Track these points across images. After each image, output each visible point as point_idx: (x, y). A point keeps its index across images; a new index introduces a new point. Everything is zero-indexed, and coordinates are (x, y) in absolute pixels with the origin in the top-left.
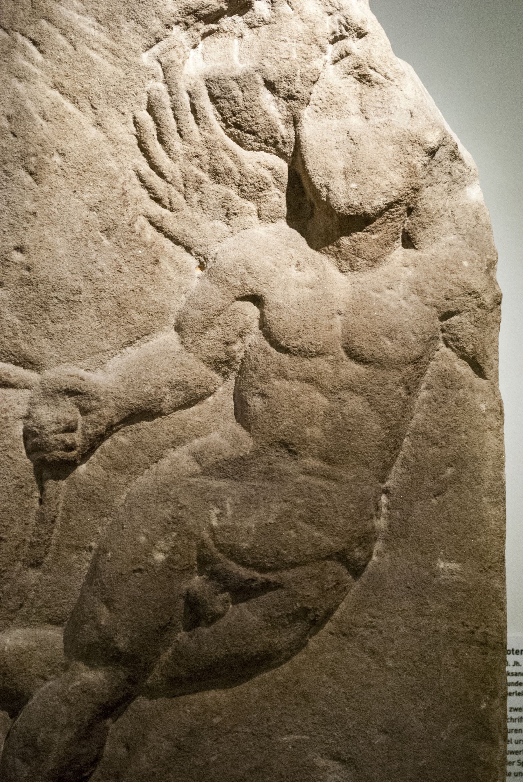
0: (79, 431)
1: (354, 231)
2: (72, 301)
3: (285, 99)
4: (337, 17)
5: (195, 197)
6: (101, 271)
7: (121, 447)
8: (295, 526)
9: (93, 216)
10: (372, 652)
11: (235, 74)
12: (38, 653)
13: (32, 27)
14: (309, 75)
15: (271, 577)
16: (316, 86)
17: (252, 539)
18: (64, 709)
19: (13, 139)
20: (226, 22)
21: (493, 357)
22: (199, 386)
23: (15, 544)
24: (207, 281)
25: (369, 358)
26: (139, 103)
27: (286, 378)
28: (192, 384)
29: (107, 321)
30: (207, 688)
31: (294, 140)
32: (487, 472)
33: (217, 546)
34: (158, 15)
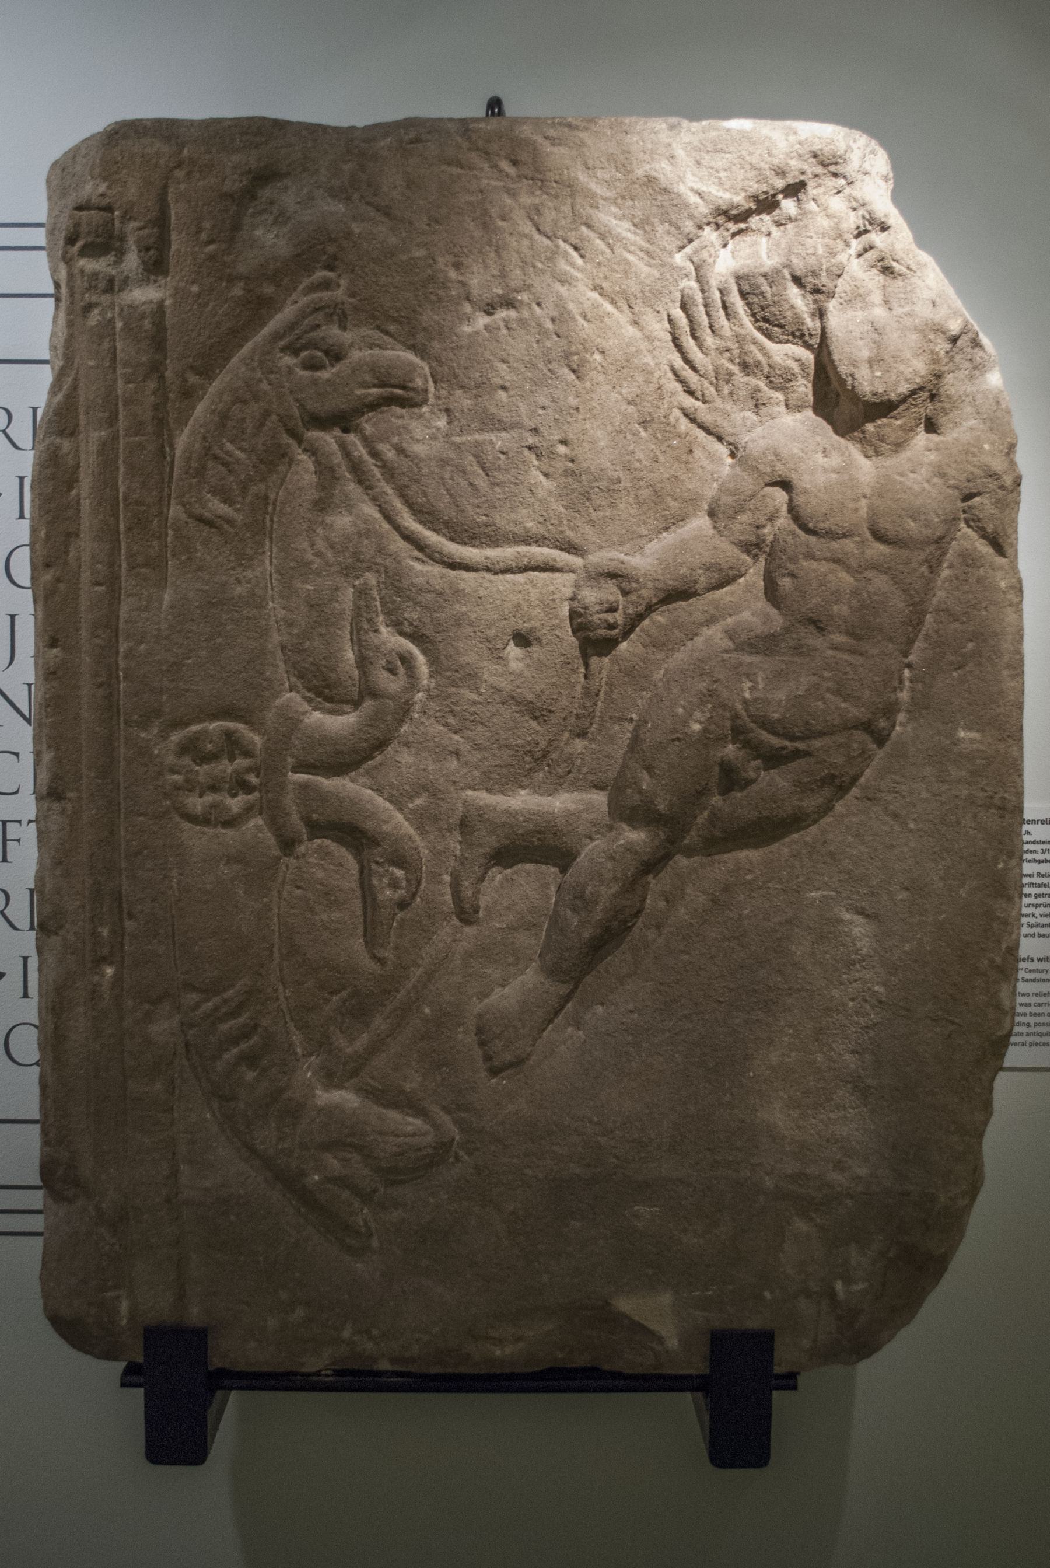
0: (620, 611)
1: (880, 417)
5: (726, 390)
6: (639, 461)
7: (660, 626)
8: (823, 698)
9: (631, 409)
12: (585, 815)
13: (573, 233)
15: (800, 745)
16: (840, 280)
17: (782, 710)
18: (609, 865)
20: (754, 221)
21: (1014, 536)
22: (731, 568)
23: (563, 715)
26: (674, 301)
27: (814, 558)
28: (725, 566)
30: (740, 848)
31: (819, 332)
33: (749, 716)
34: (691, 217)
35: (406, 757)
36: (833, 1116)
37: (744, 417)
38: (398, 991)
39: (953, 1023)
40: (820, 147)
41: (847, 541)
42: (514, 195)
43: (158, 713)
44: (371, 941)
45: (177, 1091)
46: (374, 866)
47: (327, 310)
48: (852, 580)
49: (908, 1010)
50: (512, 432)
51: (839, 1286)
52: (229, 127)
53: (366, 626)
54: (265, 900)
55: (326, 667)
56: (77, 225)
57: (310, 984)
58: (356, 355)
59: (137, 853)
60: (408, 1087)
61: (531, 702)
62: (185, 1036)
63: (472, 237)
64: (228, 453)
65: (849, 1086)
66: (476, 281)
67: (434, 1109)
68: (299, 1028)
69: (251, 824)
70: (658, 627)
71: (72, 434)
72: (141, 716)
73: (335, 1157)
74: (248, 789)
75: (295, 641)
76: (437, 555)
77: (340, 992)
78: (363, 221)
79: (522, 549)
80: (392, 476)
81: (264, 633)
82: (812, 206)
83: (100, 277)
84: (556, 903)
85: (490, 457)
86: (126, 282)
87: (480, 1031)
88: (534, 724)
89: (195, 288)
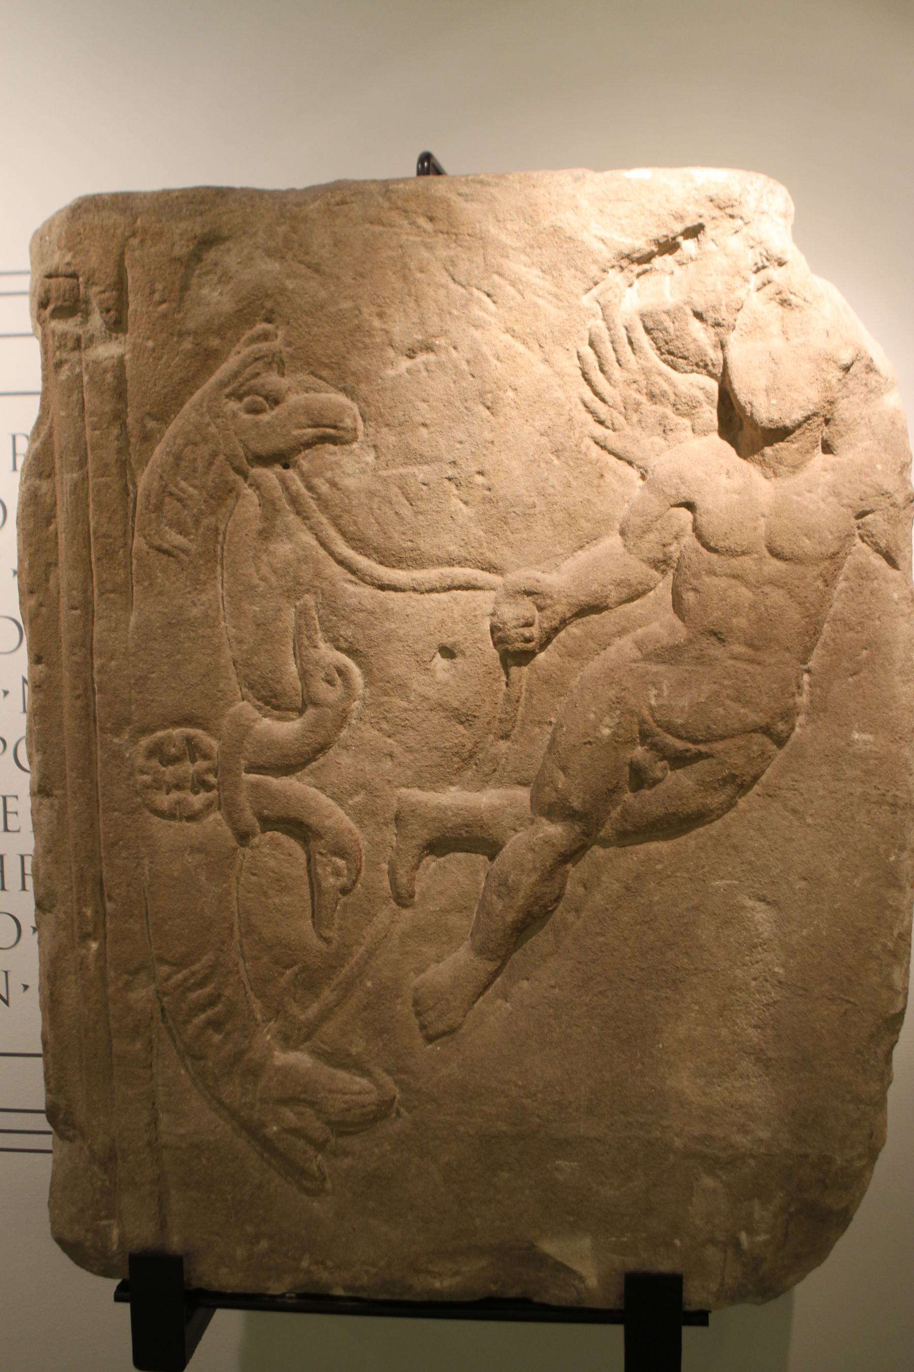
0: (536, 625)
1: (777, 442)
3: (713, 326)
4: (759, 249)
5: (635, 418)
6: (553, 487)
7: (574, 638)
8: (723, 705)
9: (544, 440)
10: (794, 811)
11: (665, 308)
12: (509, 810)
13: (486, 282)
15: (703, 748)
16: (740, 313)
17: (685, 716)
18: (530, 856)
19: (472, 379)
20: (657, 261)
21: (907, 550)
22: (640, 583)
23: (487, 720)
24: (647, 491)
25: (789, 555)
26: (582, 339)
27: (715, 574)
28: (634, 582)
29: (560, 529)
30: (650, 840)
31: (722, 362)
33: (655, 721)
34: (595, 262)
35: (345, 759)
36: (737, 1084)
37: (652, 443)
38: (343, 967)
39: (848, 1002)
40: (715, 191)
41: (745, 558)
42: (431, 248)
43: (128, 721)
44: (317, 923)
45: (155, 1051)
46: (318, 857)
47: (266, 359)
48: (750, 595)
49: (806, 990)
50: (433, 465)
51: (743, 1236)
52: (177, 197)
53: (306, 643)
54: (225, 885)
55: (272, 679)
56: (47, 291)
57: (265, 959)
58: (293, 399)
59: (114, 844)
60: (354, 1051)
61: (457, 709)
62: (161, 1002)
63: (394, 289)
64: (182, 490)
65: (752, 1057)
66: (397, 328)
67: (378, 1071)
68: (258, 997)
69: (211, 818)
70: (572, 638)
71: (49, 476)
72: (113, 724)
73: (291, 1111)
74: (208, 787)
75: (245, 656)
76: (367, 577)
77: (292, 966)
78: (296, 277)
79: (446, 570)
80: (326, 507)
81: (217, 650)
82: (711, 246)
83: (69, 336)
84: (485, 888)
85: (413, 489)
86: (91, 340)
87: (416, 1003)
88: (460, 728)
89: (150, 344)
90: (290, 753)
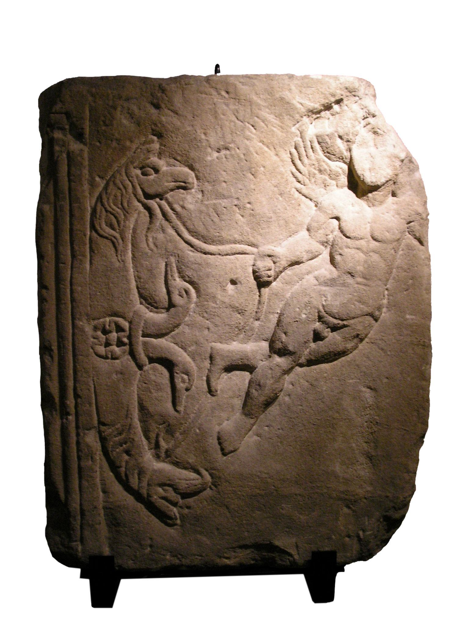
0: (273, 270)
2: (268, 221)
4: (365, 110)
5: (313, 180)
10: (382, 349)
11: (327, 133)
14: (355, 133)
15: (345, 323)
18: (270, 372)
20: (323, 114)
27: (349, 248)
28: (314, 251)
32: (425, 282)
34: (298, 113)
37: (320, 191)
44: (174, 404)
48: (364, 256)
51: (361, 533)
60: (190, 461)
63: (211, 122)
79: (233, 246)
82: (345, 108)
88: (239, 316)
90: (163, 328)
